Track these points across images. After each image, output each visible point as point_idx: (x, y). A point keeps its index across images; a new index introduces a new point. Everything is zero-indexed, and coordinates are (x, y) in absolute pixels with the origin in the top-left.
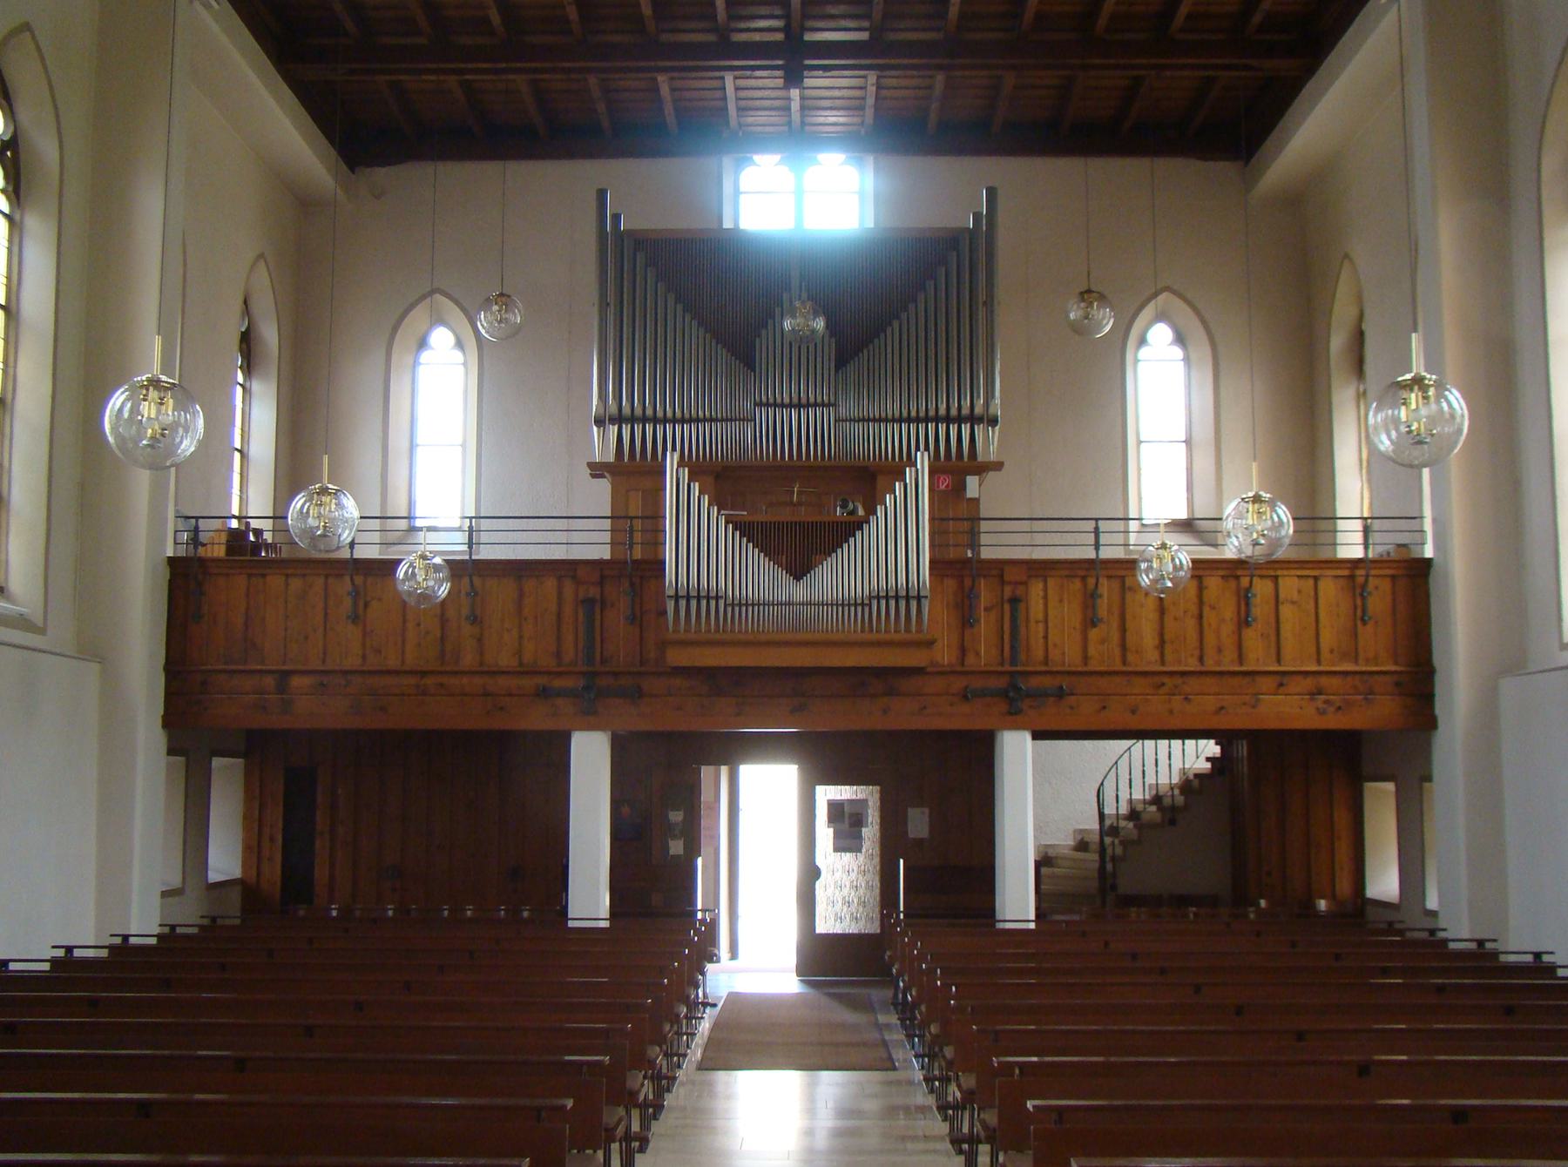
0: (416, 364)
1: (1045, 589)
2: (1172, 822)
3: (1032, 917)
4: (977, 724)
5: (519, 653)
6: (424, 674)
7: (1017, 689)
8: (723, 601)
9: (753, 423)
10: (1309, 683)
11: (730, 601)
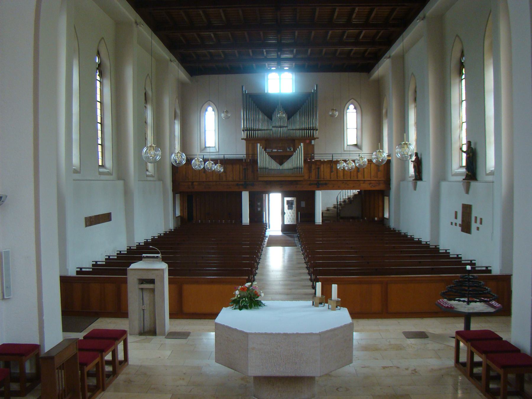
0: (205, 114)
1: (324, 166)
2: (351, 203)
3: (321, 222)
4: (312, 190)
5: (233, 178)
6: (216, 182)
7: (319, 183)
10: (369, 182)
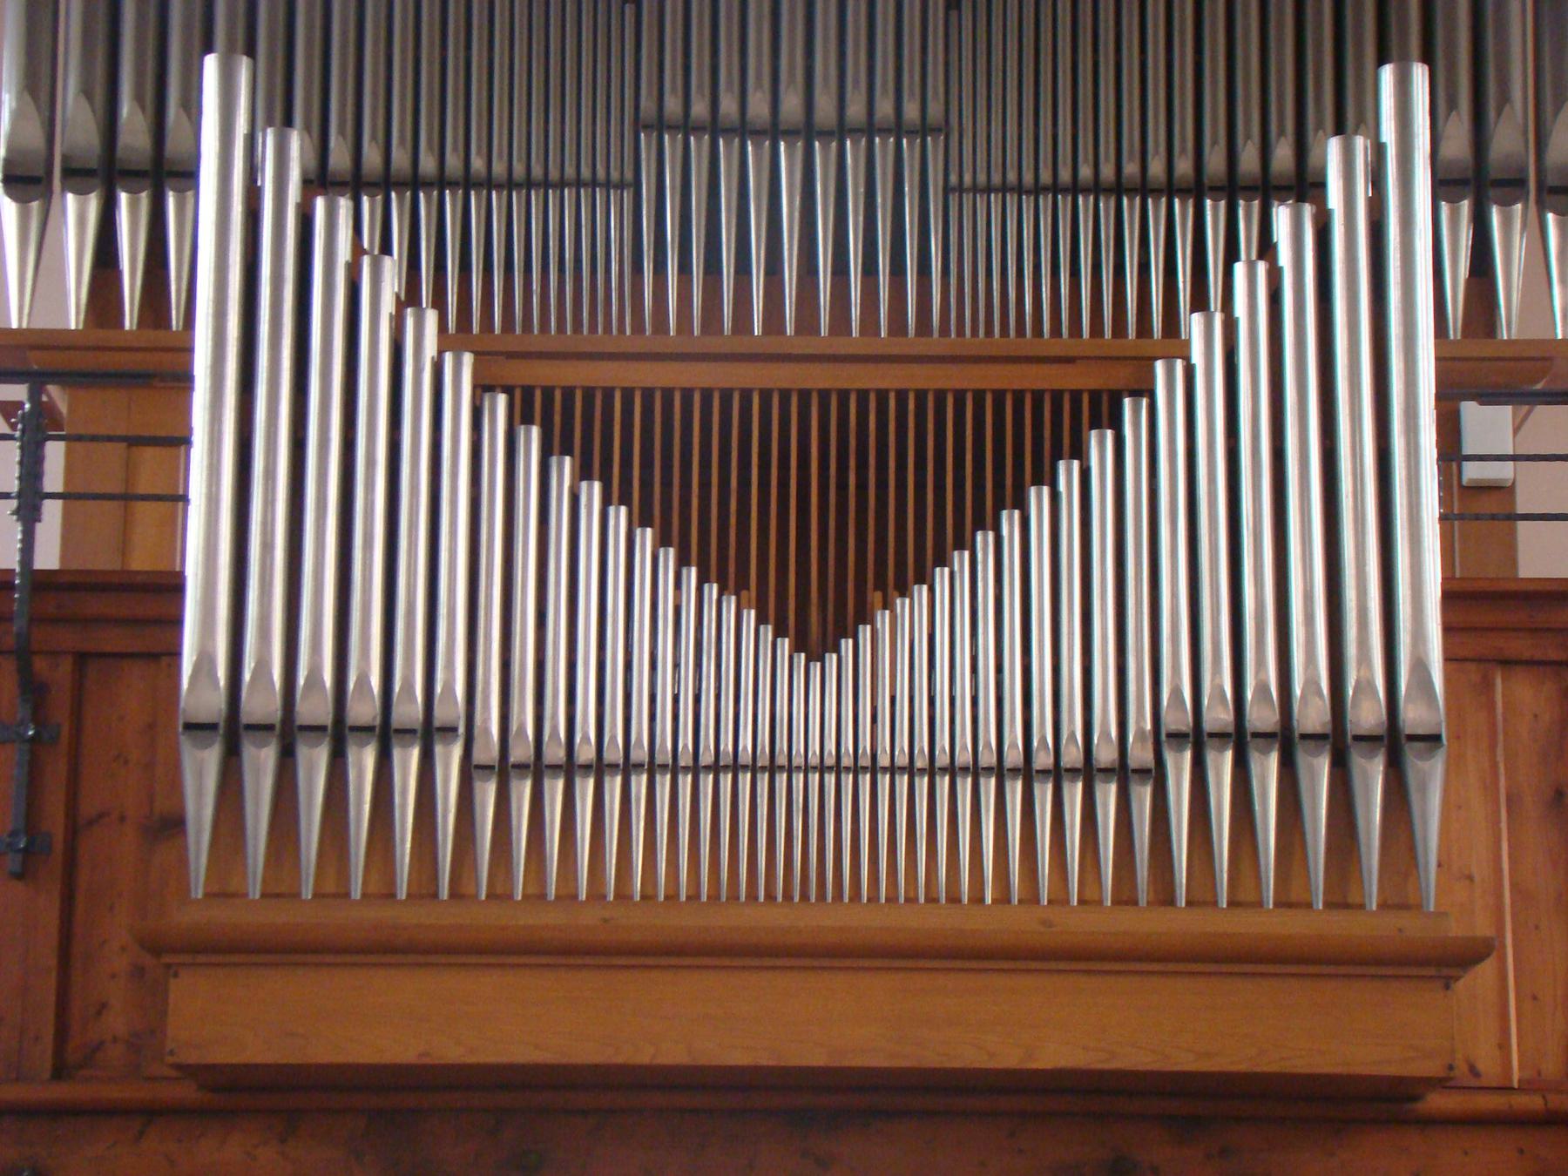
8: (457, 751)
9: (627, 196)
11: (487, 751)
